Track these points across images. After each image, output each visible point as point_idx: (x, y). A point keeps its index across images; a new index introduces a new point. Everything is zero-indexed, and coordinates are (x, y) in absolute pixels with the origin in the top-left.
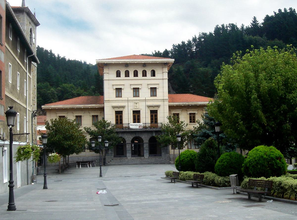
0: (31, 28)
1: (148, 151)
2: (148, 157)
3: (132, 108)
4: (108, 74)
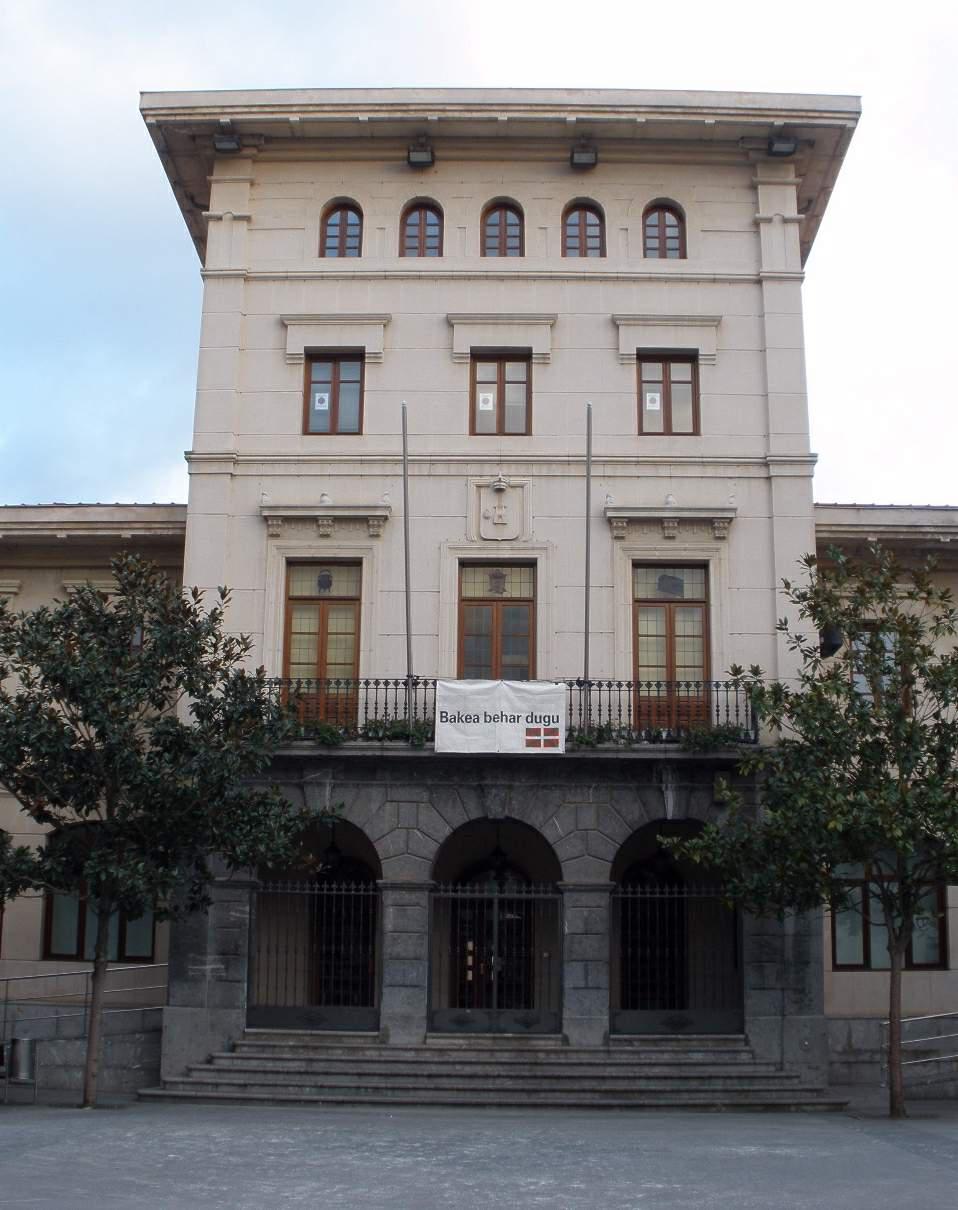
1: (601, 977)
2: (607, 1040)
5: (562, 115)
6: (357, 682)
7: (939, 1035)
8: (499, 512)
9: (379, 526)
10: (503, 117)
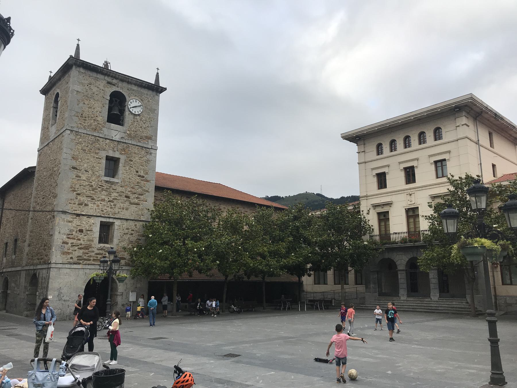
0: (106, 207)
4: (363, 153)
7: (172, 316)
8: (410, 199)
9: (391, 205)
10: (400, 122)
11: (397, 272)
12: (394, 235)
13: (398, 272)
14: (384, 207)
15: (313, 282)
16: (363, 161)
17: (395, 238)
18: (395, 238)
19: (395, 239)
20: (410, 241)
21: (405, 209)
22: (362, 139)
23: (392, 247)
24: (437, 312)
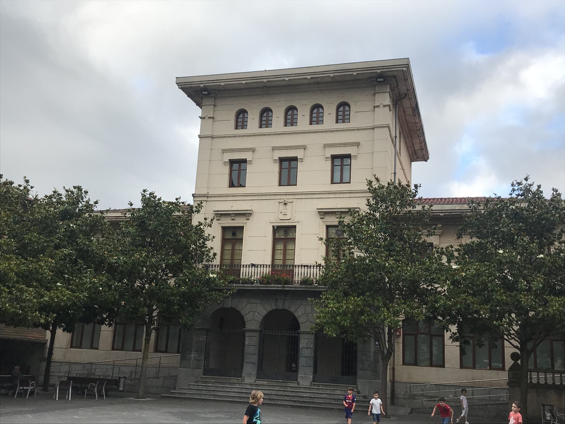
3: (273, 220)
5: (306, 77)
6: (241, 266)
9: (249, 216)
11: (244, 332)
12: (250, 269)
13: (246, 333)
14: (325, 218)
15: (69, 343)
16: (209, 133)
17: (250, 273)
18: (250, 273)
19: (250, 275)
20: (278, 282)
21: (273, 227)
22: (212, 95)
23: (243, 288)
24: (314, 407)
